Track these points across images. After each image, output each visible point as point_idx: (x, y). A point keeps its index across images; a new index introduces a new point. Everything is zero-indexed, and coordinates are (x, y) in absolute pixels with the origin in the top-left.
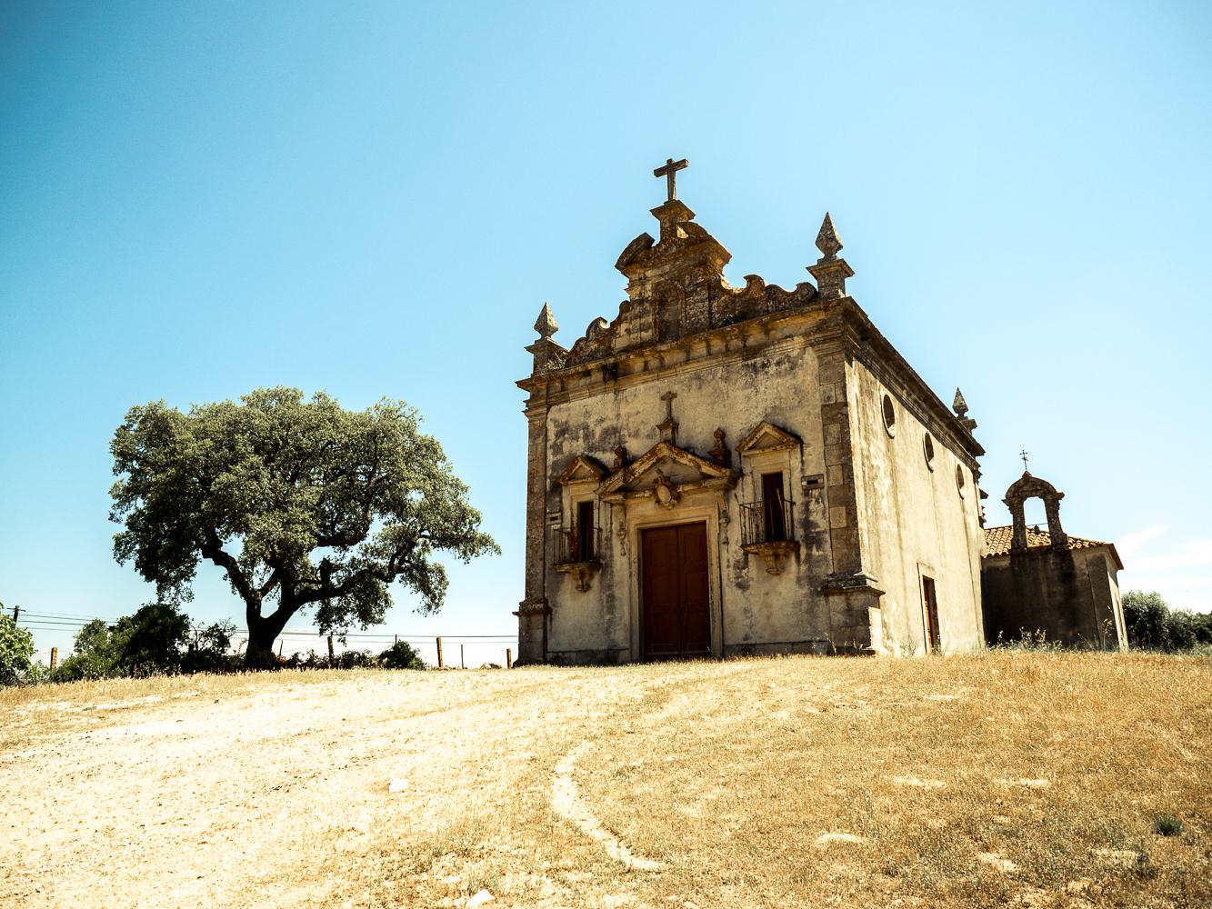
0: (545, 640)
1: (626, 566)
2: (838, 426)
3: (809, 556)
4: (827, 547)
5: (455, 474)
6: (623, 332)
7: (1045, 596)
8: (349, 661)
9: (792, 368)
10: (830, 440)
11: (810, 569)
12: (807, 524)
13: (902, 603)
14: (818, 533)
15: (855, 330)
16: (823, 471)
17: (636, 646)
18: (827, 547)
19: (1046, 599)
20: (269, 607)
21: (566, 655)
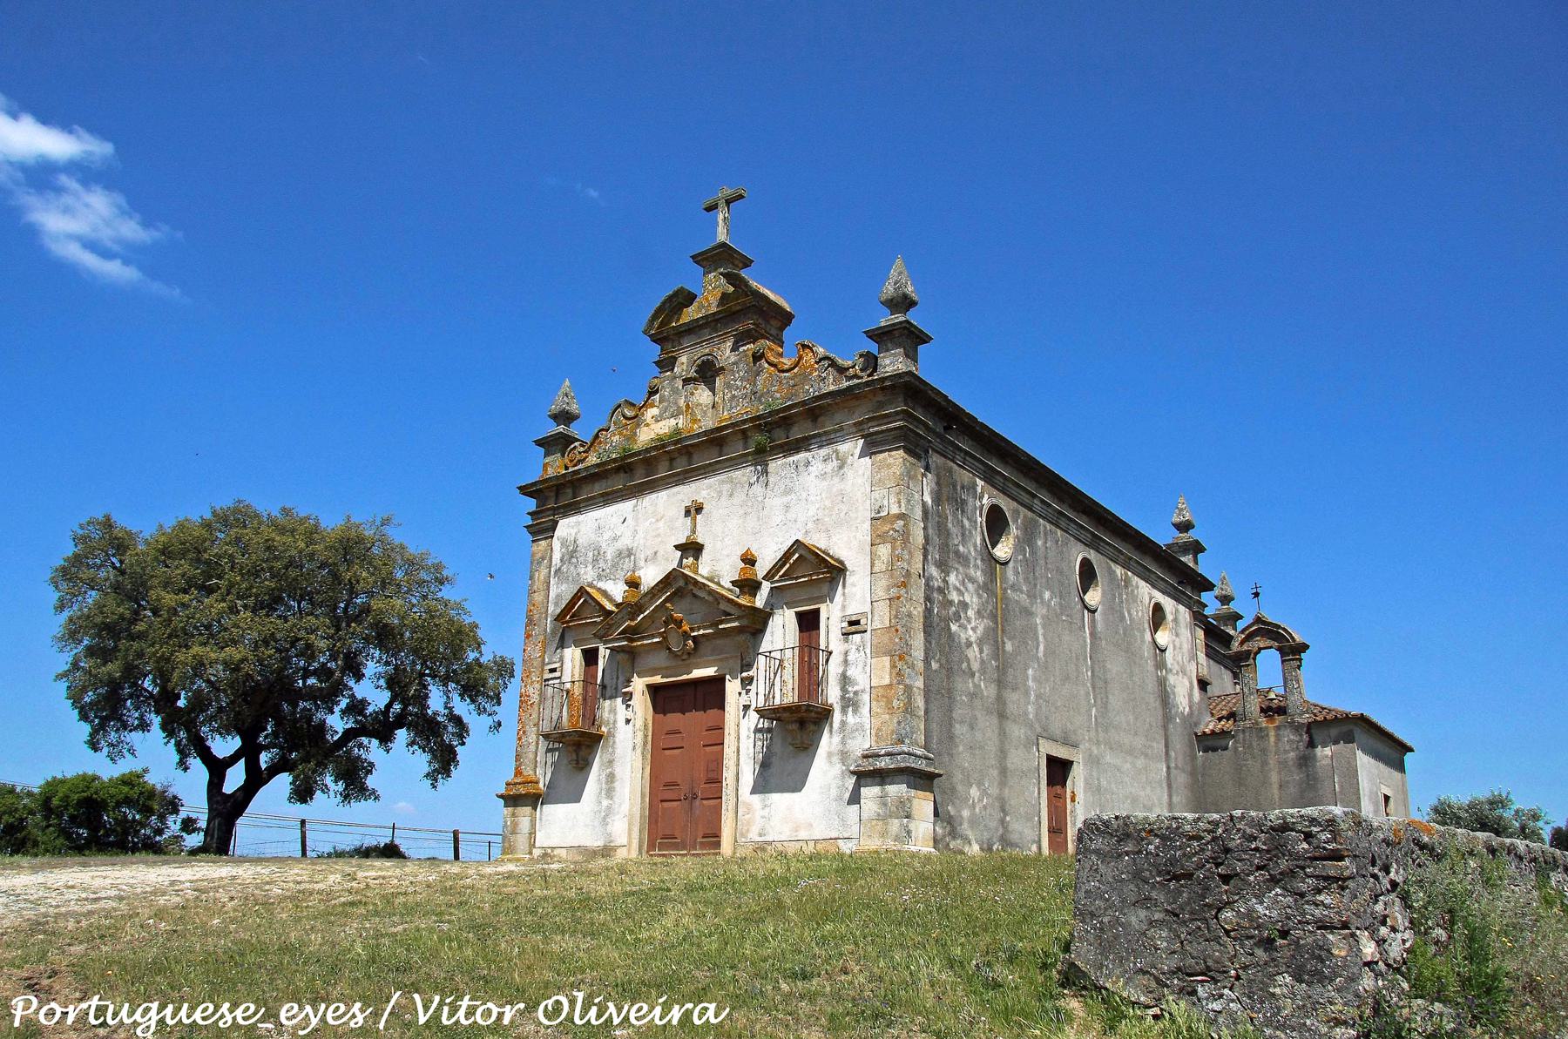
0: (532, 833)
1: (630, 735)
2: (889, 546)
3: (843, 723)
4: (865, 710)
5: (397, 542)
6: (649, 420)
7: (1276, 786)
8: (926, 712)
9: (841, 467)
10: (879, 566)
11: (843, 742)
12: (845, 680)
13: (994, 791)
14: (856, 693)
15: (397, 1003)
16: (867, 608)
17: (635, 842)
18: (865, 710)
19: (1276, 791)
20: (235, 778)
21: (556, 852)
